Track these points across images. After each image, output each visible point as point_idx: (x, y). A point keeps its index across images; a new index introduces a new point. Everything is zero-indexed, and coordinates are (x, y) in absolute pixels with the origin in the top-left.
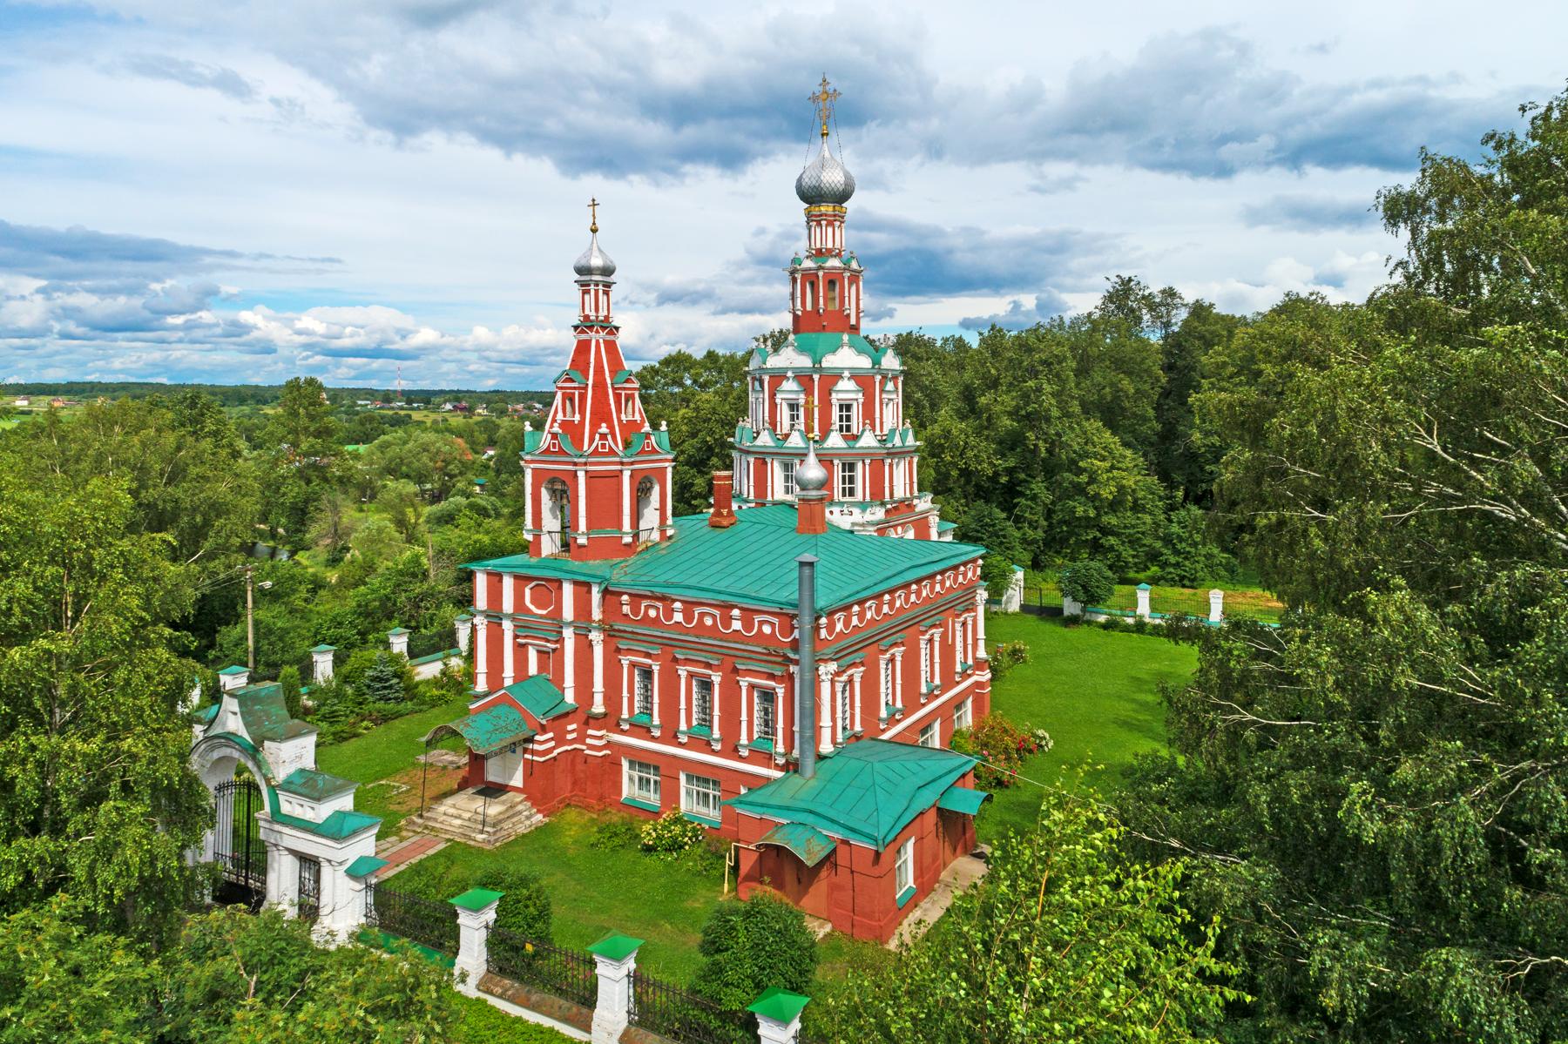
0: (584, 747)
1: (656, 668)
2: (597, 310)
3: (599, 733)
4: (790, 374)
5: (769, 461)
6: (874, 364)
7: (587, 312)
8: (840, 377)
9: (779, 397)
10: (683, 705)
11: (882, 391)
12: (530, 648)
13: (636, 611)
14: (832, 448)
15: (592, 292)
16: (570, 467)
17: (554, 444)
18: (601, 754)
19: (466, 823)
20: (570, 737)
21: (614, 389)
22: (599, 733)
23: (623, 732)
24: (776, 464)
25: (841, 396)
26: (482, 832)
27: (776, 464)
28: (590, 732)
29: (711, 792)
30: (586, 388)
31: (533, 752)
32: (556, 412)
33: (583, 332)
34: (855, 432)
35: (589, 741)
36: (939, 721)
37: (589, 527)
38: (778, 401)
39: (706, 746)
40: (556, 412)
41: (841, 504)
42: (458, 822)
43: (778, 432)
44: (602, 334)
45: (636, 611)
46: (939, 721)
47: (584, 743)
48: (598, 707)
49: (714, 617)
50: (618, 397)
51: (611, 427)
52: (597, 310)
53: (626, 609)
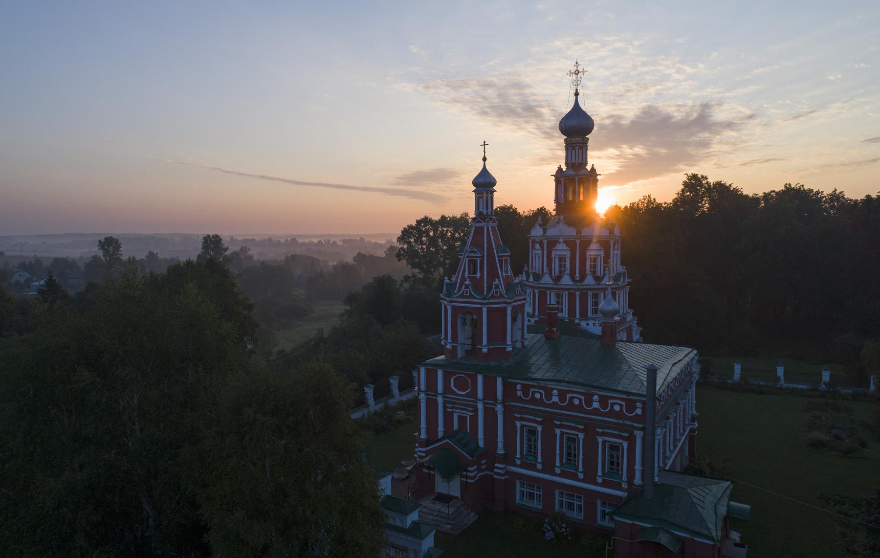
0: (493, 474)
1: (540, 428)
2: (487, 208)
3: (502, 466)
4: (561, 240)
5: (548, 292)
6: (577, 233)
7: (481, 210)
8: (559, 242)
9: (554, 253)
10: (558, 452)
11: (614, 249)
12: (455, 414)
13: (526, 395)
14: (587, 285)
15: (485, 198)
16: (479, 306)
17: (467, 291)
18: (503, 478)
19: (436, 518)
20: (483, 467)
21: (498, 257)
22: (502, 466)
23: (516, 466)
24: (553, 294)
25: (558, 253)
26: (448, 524)
27: (553, 294)
28: (496, 465)
29: (536, 492)
30: (483, 257)
31: (467, 477)
32: (464, 271)
33: (478, 222)
34: (598, 274)
35: (495, 470)
36: (554, 421)
37: (488, 341)
38: (553, 256)
39: (533, 467)
40: (464, 271)
41: (592, 318)
42: (431, 517)
43: (553, 275)
44: (490, 223)
45: (526, 395)
46: (554, 421)
47: (493, 472)
48: (500, 451)
49: (580, 400)
50: (501, 261)
51: (499, 281)
52: (487, 208)
53: (519, 393)
